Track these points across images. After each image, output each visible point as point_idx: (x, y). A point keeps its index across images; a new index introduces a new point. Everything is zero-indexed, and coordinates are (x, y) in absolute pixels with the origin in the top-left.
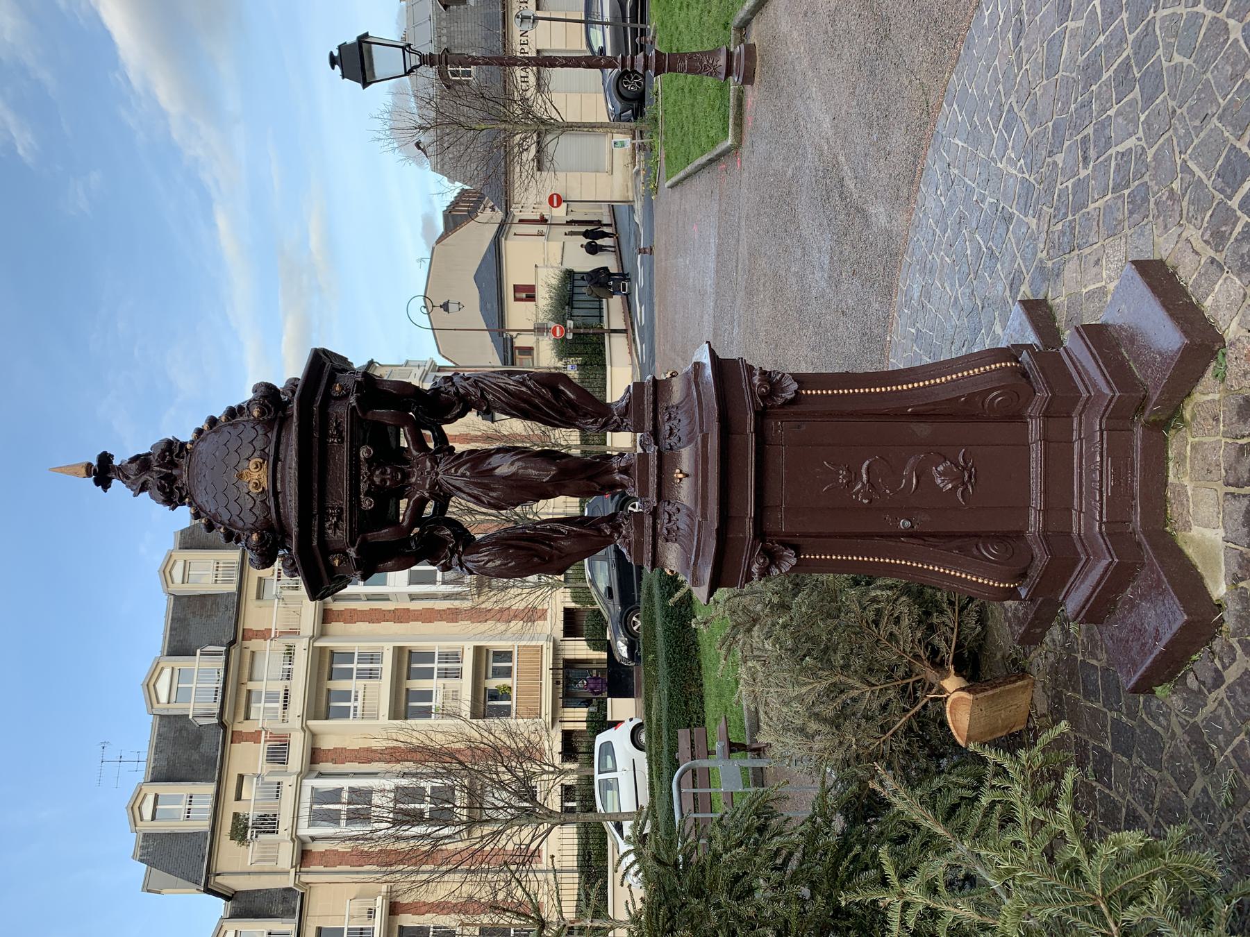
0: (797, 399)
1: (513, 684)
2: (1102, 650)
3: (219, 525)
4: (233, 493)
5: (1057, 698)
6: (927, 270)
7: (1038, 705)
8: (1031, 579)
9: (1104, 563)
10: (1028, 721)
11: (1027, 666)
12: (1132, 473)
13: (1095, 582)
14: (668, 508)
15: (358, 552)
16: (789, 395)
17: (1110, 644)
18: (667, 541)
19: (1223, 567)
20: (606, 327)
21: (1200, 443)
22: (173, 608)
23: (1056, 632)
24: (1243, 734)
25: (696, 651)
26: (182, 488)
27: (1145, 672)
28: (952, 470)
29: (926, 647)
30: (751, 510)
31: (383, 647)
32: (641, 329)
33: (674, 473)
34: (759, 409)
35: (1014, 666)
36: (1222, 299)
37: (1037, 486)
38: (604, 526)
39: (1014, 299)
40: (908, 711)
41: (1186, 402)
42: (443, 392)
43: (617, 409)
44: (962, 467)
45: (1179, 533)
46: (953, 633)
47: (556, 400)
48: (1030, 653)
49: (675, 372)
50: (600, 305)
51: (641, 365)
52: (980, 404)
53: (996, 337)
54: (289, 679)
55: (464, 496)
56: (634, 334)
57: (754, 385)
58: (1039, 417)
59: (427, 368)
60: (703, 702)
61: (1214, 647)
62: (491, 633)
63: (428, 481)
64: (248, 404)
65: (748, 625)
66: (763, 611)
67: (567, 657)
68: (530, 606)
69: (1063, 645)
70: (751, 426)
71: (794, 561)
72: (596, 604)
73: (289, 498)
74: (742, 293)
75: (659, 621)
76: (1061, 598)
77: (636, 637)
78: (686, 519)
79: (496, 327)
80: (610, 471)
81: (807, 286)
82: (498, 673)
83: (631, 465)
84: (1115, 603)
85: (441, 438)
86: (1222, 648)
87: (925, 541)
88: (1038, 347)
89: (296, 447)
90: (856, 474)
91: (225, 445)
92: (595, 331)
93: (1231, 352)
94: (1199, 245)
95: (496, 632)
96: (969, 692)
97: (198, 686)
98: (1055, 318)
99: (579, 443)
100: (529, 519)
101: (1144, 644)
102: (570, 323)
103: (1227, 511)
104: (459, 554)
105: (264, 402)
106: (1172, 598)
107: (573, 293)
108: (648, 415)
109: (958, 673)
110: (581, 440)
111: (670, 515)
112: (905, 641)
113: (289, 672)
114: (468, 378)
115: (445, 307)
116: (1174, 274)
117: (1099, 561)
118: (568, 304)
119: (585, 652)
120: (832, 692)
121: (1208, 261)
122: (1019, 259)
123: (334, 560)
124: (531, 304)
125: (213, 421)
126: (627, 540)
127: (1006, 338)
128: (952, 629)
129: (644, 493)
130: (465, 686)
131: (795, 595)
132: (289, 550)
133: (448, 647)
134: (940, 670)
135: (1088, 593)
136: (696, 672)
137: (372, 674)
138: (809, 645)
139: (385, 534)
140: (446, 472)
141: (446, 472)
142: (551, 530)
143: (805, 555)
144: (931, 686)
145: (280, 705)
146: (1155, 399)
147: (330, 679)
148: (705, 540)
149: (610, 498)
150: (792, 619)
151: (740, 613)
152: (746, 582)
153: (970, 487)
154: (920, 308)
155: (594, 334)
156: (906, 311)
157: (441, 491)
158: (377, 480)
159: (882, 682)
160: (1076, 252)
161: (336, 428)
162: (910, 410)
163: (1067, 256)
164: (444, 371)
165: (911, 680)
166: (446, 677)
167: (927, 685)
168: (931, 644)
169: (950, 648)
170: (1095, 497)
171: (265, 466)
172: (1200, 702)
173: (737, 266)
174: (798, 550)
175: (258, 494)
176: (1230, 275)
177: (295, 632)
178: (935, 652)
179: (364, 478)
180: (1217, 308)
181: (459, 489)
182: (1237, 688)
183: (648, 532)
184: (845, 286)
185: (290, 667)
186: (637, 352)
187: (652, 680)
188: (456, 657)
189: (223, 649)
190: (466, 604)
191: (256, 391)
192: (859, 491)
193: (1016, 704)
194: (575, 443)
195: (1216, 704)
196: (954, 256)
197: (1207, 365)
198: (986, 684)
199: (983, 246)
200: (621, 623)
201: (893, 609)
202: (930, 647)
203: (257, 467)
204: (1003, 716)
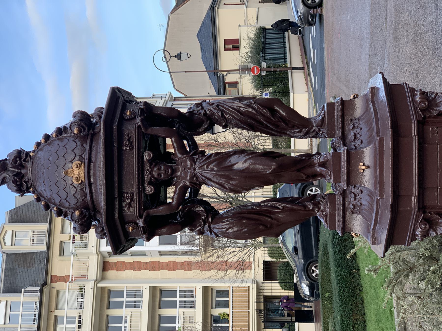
1: (230, 312)
3: (53, 206)
4: (62, 185)
15: (145, 222)
18: (353, 213)
22: (6, 261)
25: (360, 290)
26: (28, 182)
30: (416, 191)
31: (142, 287)
32: (314, 66)
33: (359, 166)
34: (421, 119)
38: (308, 203)
42: (196, 114)
47: (273, 117)
49: (356, 95)
51: (315, 92)
54: (81, 309)
55: (213, 184)
56: (309, 70)
59: (167, 99)
60: (365, 326)
62: (214, 278)
63: (189, 174)
64: (70, 126)
65: (407, 272)
66: (417, 262)
67: (267, 294)
68: (240, 260)
70: (414, 131)
72: (286, 258)
73: (99, 187)
74: (391, 38)
77: (315, 281)
78: (368, 198)
79: (212, 69)
80: (312, 165)
82: (220, 305)
83: (328, 161)
85: (194, 145)
89: (104, 153)
91: (56, 152)
92: (282, 69)
95: (218, 277)
97: (23, 313)
100: (239, 200)
102: (264, 64)
104: (209, 223)
105: (81, 123)
108: (338, 126)
110: (273, 145)
111: (355, 195)
113: (82, 304)
114: (213, 104)
115: (179, 57)
118: (262, 51)
119: (278, 291)
123: (128, 227)
124: (237, 52)
125: (47, 137)
126: (324, 213)
129: (337, 180)
130: (198, 312)
132: (99, 221)
133: (185, 287)
136: (360, 305)
137: (136, 305)
139: (161, 210)
140: (201, 168)
141: (201, 168)
142: (272, 207)
145: (76, 326)
147: (108, 308)
148: (382, 212)
149: (294, 187)
151: (401, 264)
152: (412, 241)
155: (281, 71)
157: (197, 181)
158: (155, 174)
161: (128, 140)
164: (178, 100)
166: (185, 307)
171: (82, 166)
173: (386, 19)
175: (79, 185)
177: (85, 277)
179: (147, 173)
181: (210, 179)
183: (339, 207)
185: (82, 300)
187: (329, 311)
188: (192, 294)
189: (38, 288)
190: (197, 259)
191: (75, 117)
200: (304, 271)
203: (77, 167)
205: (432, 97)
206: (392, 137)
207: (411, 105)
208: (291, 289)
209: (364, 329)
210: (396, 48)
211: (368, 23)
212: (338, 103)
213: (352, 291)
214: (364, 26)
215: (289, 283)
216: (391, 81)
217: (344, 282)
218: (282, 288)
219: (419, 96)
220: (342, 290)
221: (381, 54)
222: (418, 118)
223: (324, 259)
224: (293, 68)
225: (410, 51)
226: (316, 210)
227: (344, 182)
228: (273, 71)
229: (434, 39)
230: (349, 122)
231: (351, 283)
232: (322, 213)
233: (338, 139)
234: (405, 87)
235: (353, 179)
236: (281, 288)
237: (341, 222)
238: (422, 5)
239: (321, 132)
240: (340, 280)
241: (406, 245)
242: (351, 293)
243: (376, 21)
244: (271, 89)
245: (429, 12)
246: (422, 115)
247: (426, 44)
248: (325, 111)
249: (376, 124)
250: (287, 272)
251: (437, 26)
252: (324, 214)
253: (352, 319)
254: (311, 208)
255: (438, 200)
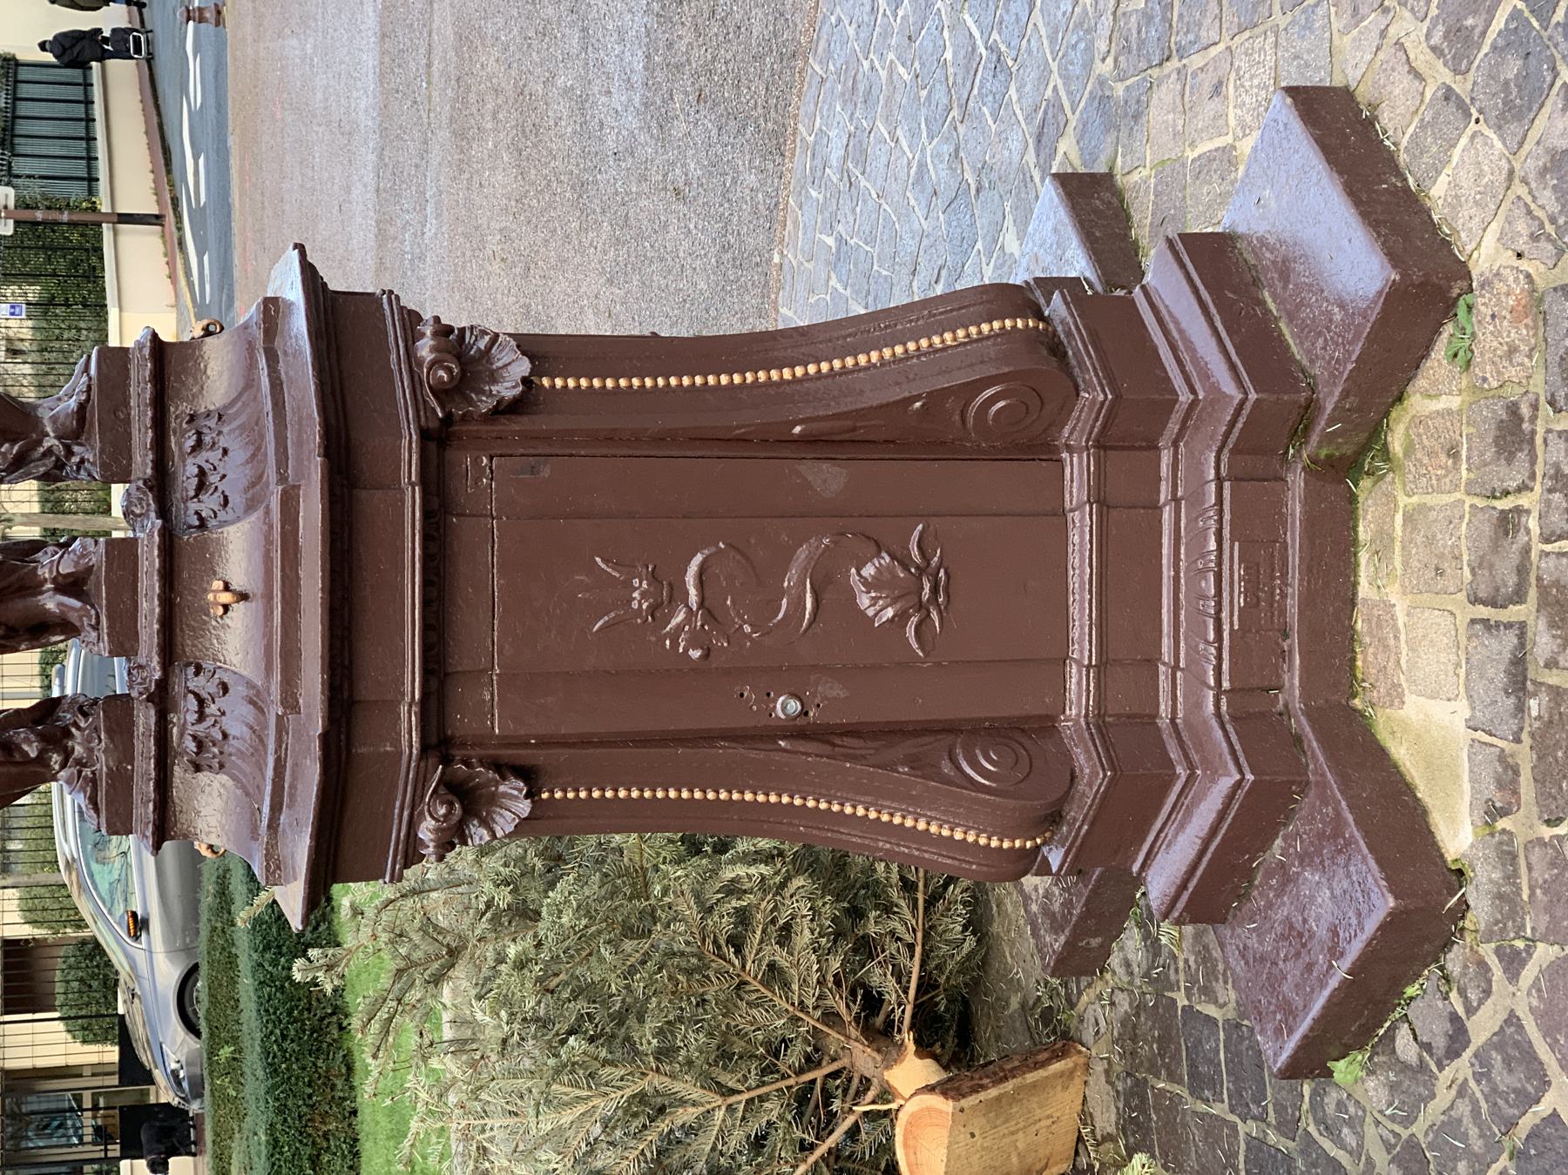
0: (527, 401)
2: (1226, 982)
5: (1135, 1098)
6: (858, 94)
7: (1097, 1115)
8: (1071, 825)
9: (1225, 783)
10: (1077, 1153)
11: (1074, 1023)
12: (1284, 575)
13: (1206, 829)
14: (196, 683)
16: (508, 389)
17: (1239, 967)
18: (198, 768)
19: (1467, 786)
20: (105, 208)
21: (1422, 509)
23: (1131, 942)
24: (1505, 1156)
27: (1311, 1029)
28: (895, 576)
29: (853, 993)
30: (412, 683)
33: (206, 591)
34: (434, 425)
35: (1046, 1026)
36: (1466, 182)
37: (1082, 609)
39: (1044, 172)
40: (812, 1147)
41: (1394, 414)
43: (54, 419)
44: (917, 568)
45: (1380, 712)
46: (912, 957)
48: (1080, 994)
50: (89, 150)
52: (957, 417)
53: (1006, 260)
56: (180, 229)
57: (420, 364)
58: (1088, 449)
60: (357, 1155)
61: (1449, 966)
65: (436, 965)
66: (473, 927)
69: (1147, 975)
71: (524, 807)
72: (87, 926)
74: (444, 135)
75: (245, 963)
76: (1135, 868)
78: (247, 711)
81: (595, 124)
83: (89, 570)
84: (1249, 874)
86: (1466, 967)
87: (834, 745)
88: (1091, 286)
90: (671, 586)
92: (76, 217)
93: (1483, 303)
94: (1421, 56)
96: (945, 1094)
98: (1128, 218)
99: (36, 508)
101: (1309, 967)
103: (1474, 660)
106: (1364, 858)
107: (15, 117)
109: (924, 1048)
110: (44, 501)
111: (201, 702)
112: (804, 982)
116: (1371, 122)
117: (1214, 781)
119: (61, 1049)
120: (635, 1115)
121: (1440, 93)
122: (1055, 75)
126: (87, 772)
127: (1024, 262)
128: (911, 947)
131: (552, 885)
134: (882, 1042)
135: (1191, 854)
136: (339, 1083)
138: (582, 1005)
143: (552, 792)
144: (866, 1083)
146: (1329, 407)
148: (296, 765)
150: (539, 945)
151: (416, 938)
152: (406, 866)
153: (934, 615)
154: (844, 186)
155: (73, 224)
156: (814, 194)
159: (752, 1082)
160: (1174, 63)
162: (797, 429)
163: (1155, 72)
165: (818, 1074)
167: (856, 1081)
168: (864, 986)
169: (906, 992)
170: (1206, 633)
172: (1421, 1089)
173: (429, 66)
174: (531, 777)
176: (1482, 127)
178: (872, 1001)
180: (1456, 202)
182: (1494, 1054)
184: (680, 128)
186: (188, 273)
192: (680, 628)
193: (1049, 1117)
194: (25, 508)
195: (1453, 1092)
196: (917, 65)
197: (1436, 331)
198: (981, 1072)
199: (979, 42)
201: (775, 908)
202: (860, 992)
204: (1020, 1145)
205: (479, 349)
206: (326, 487)
207: (401, 373)
208: (106, 1039)
209: (351, 1168)
210: (462, 171)
211: (371, 76)
212: (141, 350)
213: (312, 1034)
214: (359, 83)
215: (99, 1016)
216: (335, 284)
217: (284, 1003)
218: (74, 1037)
219: (432, 343)
220: (278, 1032)
221: (413, 188)
222: (423, 419)
223: (219, 925)
224: (119, 215)
225: (504, 187)
226: (56, 758)
227: (150, 652)
228: (43, 223)
229: (577, 150)
230: (184, 426)
231: (311, 1004)
232: (80, 772)
233: (138, 489)
234: (386, 306)
235: (187, 645)
236: (69, 1037)
237: (151, 806)
238: (540, 28)
239: (75, 459)
240: (269, 996)
241: (387, 880)
242: (307, 1041)
243: (396, 70)
244: (33, 292)
245: (562, 54)
246: (438, 410)
247: (552, 164)
248: (90, 379)
249: (276, 438)
250: (93, 978)
251: (587, 105)
252: (86, 777)
253: (310, 1135)
254: (33, 755)
255: (493, 715)
